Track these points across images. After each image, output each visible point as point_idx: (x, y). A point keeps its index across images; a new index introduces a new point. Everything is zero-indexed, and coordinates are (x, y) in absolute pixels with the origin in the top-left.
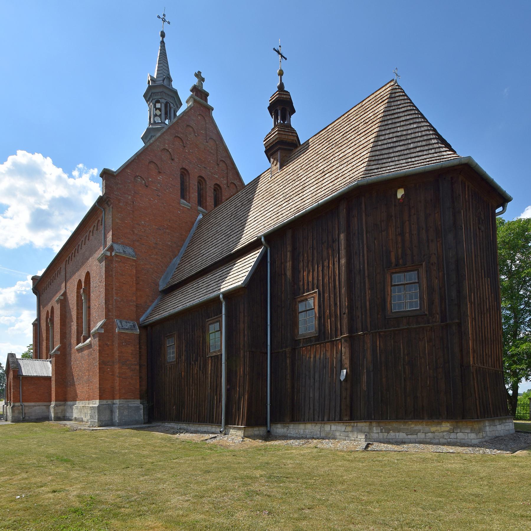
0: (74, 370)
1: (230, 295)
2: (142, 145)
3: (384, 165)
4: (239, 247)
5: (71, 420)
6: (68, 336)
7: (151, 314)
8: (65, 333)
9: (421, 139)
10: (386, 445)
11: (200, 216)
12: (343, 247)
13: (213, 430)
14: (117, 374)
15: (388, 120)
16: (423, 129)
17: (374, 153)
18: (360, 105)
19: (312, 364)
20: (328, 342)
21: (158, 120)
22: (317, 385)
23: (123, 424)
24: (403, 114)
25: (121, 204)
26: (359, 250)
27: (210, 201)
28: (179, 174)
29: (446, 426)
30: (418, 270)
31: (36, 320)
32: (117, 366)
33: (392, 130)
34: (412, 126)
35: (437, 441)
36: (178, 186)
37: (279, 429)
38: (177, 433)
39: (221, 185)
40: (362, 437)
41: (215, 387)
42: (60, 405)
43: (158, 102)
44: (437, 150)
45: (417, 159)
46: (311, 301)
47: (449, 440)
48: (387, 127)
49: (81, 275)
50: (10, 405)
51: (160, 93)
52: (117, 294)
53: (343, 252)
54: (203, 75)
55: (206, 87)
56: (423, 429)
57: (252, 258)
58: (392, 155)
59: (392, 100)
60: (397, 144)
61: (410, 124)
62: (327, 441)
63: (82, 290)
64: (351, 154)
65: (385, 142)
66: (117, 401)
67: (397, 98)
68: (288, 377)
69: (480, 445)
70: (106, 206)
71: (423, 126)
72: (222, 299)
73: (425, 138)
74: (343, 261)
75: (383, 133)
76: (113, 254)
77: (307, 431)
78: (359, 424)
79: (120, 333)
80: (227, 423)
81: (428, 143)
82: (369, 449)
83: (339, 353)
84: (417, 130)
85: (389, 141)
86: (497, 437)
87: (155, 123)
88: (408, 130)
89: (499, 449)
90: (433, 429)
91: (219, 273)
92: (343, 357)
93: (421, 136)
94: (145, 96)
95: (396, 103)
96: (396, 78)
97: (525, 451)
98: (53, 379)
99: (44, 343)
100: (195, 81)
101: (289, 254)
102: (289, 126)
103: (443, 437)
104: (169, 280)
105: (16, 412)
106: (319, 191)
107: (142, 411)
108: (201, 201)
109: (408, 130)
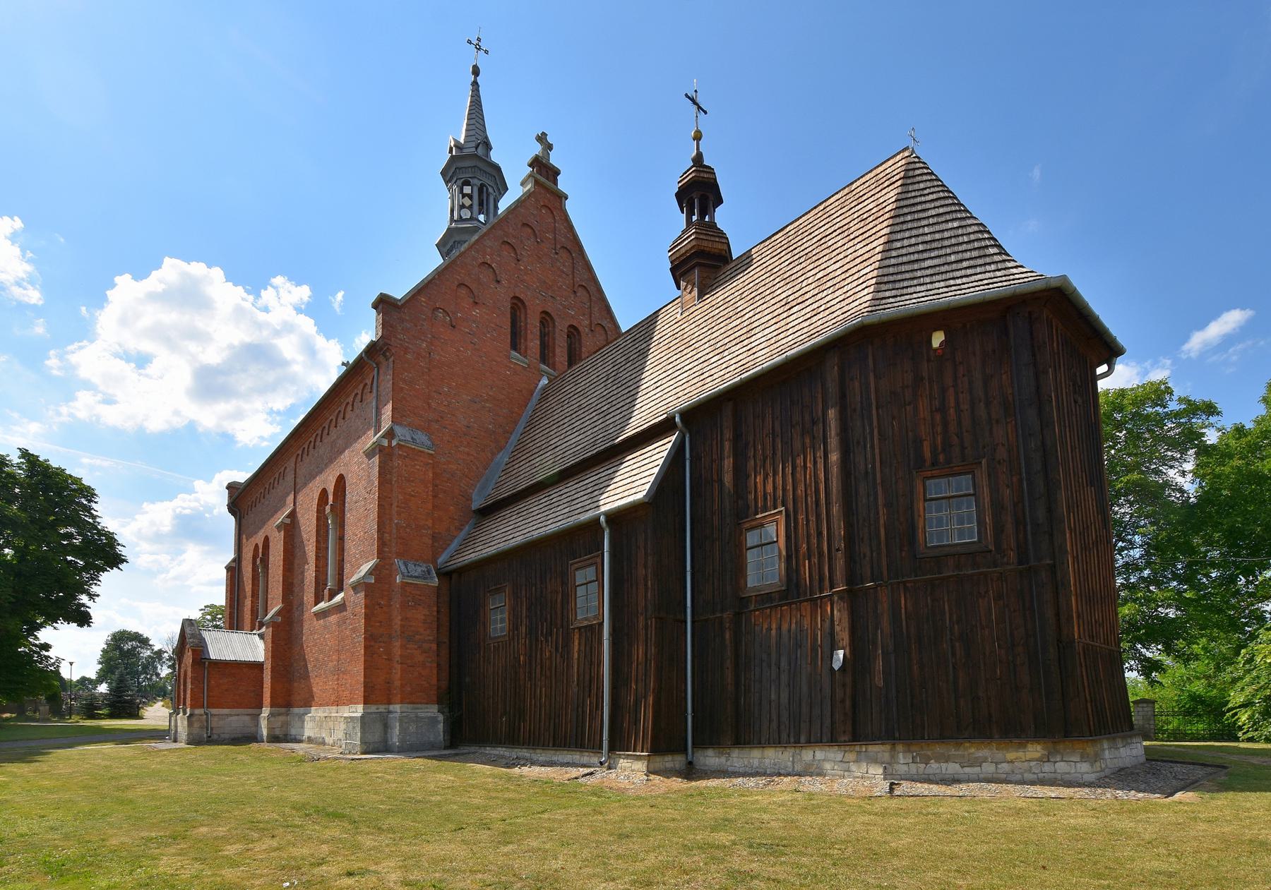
0: (307, 650)
1: (618, 518)
2: (437, 261)
3: (905, 291)
4: (629, 432)
5: (300, 741)
6: (296, 590)
7: (458, 551)
8: (292, 584)
9: (969, 247)
10: (926, 786)
11: (544, 381)
12: (833, 433)
13: (585, 759)
14: (397, 658)
15: (905, 213)
16: (970, 230)
17: (886, 271)
18: (846, 191)
19: (773, 641)
20: (807, 600)
21: (466, 214)
22: (784, 678)
23: (409, 749)
24: (932, 205)
25: (409, 356)
26: (865, 438)
27: (561, 354)
28: (508, 306)
29: (1035, 750)
30: (972, 473)
31: (234, 560)
32: (397, 644)
33: (914, 232)
34: (950, 225)
35: (1019, 777)
36: (507, 329)
37: (710, 758)
38: (514, 765)
39: (580, 329)
40: (877, 771)
41: (587, 683)
42: (279, 715)
43: (467, 183)
44: (1000, 266)
45: (964, 280)
46: (771, 529)
47: (1041, 775)
48: (905, 227)
49: (327, 480)
50: (185, 713)
51: (471, 169)
52: (399, 514)
53: (833, 442)
54: (550, 140)
55: (555, 159)
56: (989, 755)
57: (656, 456)
58: (919, 274)
59: (909, 181)
60: (926, 255)
61: (947, 221)
62: (809, 778)
63: (328, 509)
64: (839, 272)
65: (904, 251)
66: (397, 708)
67: (919, 179)
68: (728, 664)
69: (1100, 783)
70: (381, 358)
71: (970, 225)
72: (604, 525)
73: (976, 245)
74: (834, 457)
75: (899, 236)
76: (394, 443)
77: (767, 761)
78: (870, 748)
79: (404, 585)
80: (612, 748)
81: (982, 252)
82: (896, 793)
83: (828, 622)
84: (960, 231)
85: (912, 250)
86: (1121, 769)
87: (461, 219)
88: (943, 231)
89: (1140, 791)
90: (1011, 755)
91: (591, 479)
92: (837, 628)
93: (969, 242)
94: (443, 173)
95: (916, 187)
96: (912, 144)
97: (1190, 794)
98: (268, 667)
99: (248, 603)
100: (537, 149)
101: (727, 445)
102: (713, 225)
103: (1030, 771)
104: (490, 491)
105: (196, 725)
106: (782, 336)
107: (441, 726)
108: (545, 355)
109: (943, 231)
